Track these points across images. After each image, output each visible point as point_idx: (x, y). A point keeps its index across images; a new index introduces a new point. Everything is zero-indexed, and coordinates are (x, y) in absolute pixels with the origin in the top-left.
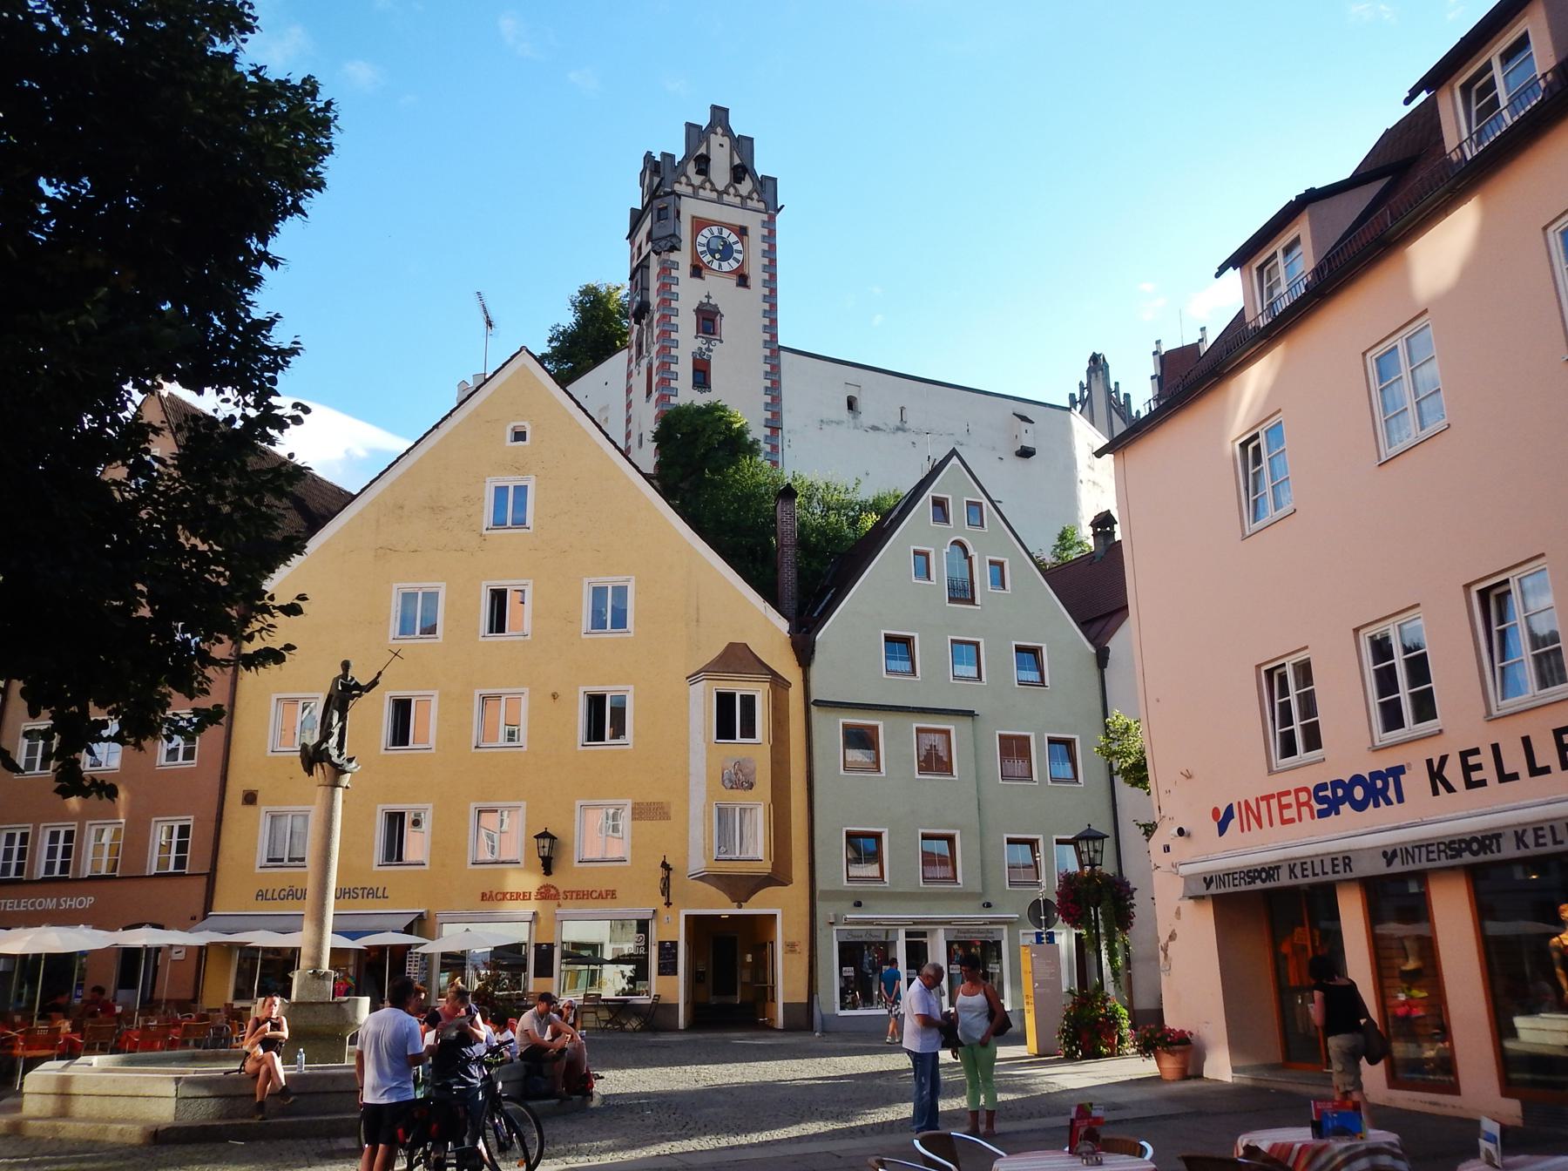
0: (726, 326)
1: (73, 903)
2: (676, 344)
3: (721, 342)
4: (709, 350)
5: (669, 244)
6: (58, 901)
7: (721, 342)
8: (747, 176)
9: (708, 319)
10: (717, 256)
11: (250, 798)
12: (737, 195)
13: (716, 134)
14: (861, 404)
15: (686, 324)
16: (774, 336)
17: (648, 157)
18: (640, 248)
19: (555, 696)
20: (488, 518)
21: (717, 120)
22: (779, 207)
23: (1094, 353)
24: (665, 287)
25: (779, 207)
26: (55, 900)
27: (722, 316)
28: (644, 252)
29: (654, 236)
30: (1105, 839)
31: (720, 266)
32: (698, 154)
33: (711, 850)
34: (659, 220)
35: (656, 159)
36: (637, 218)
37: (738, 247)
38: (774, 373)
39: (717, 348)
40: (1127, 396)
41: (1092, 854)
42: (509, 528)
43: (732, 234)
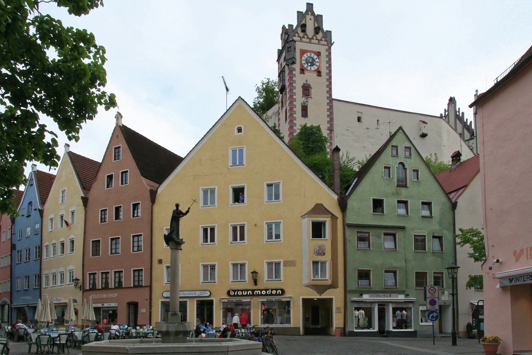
0: (313, 92)
2: (295, 106)
3: (311, 98)
4: (307, 102)
5: (292, 61)
6: (107, 295)
7: (311, 98)
8: (320, 31)
9: (306, 89)
10: (309, 64)
11: (160, 261)
12: (317, 39)
13: (308, 14)
14: (363, 119)
15: (298, 92)
16: (331, 95)
17: (284, 27)
18: (281, 64)
19: (255, 225)
20: (230, 163)
21: (309, 9)
22: (332, 43)
23: (451, 97)
24: (291, 78)
25: (332, 43)
26: (106, 295)
27: (312, 88)
28: (283, 66)
29: (286, 59)
30: (459, 269)
31: (311, 68)
32: (302, 23)
33: (310, 277)
34: (288, 52)
35: (286, 28)
36: (280, 53)
37: (317, 60)
38: (331, 107)
39: (310, 100)
40: (463, 113)
41: (453, 273)
42: (238, 165)
43: (315, 55)
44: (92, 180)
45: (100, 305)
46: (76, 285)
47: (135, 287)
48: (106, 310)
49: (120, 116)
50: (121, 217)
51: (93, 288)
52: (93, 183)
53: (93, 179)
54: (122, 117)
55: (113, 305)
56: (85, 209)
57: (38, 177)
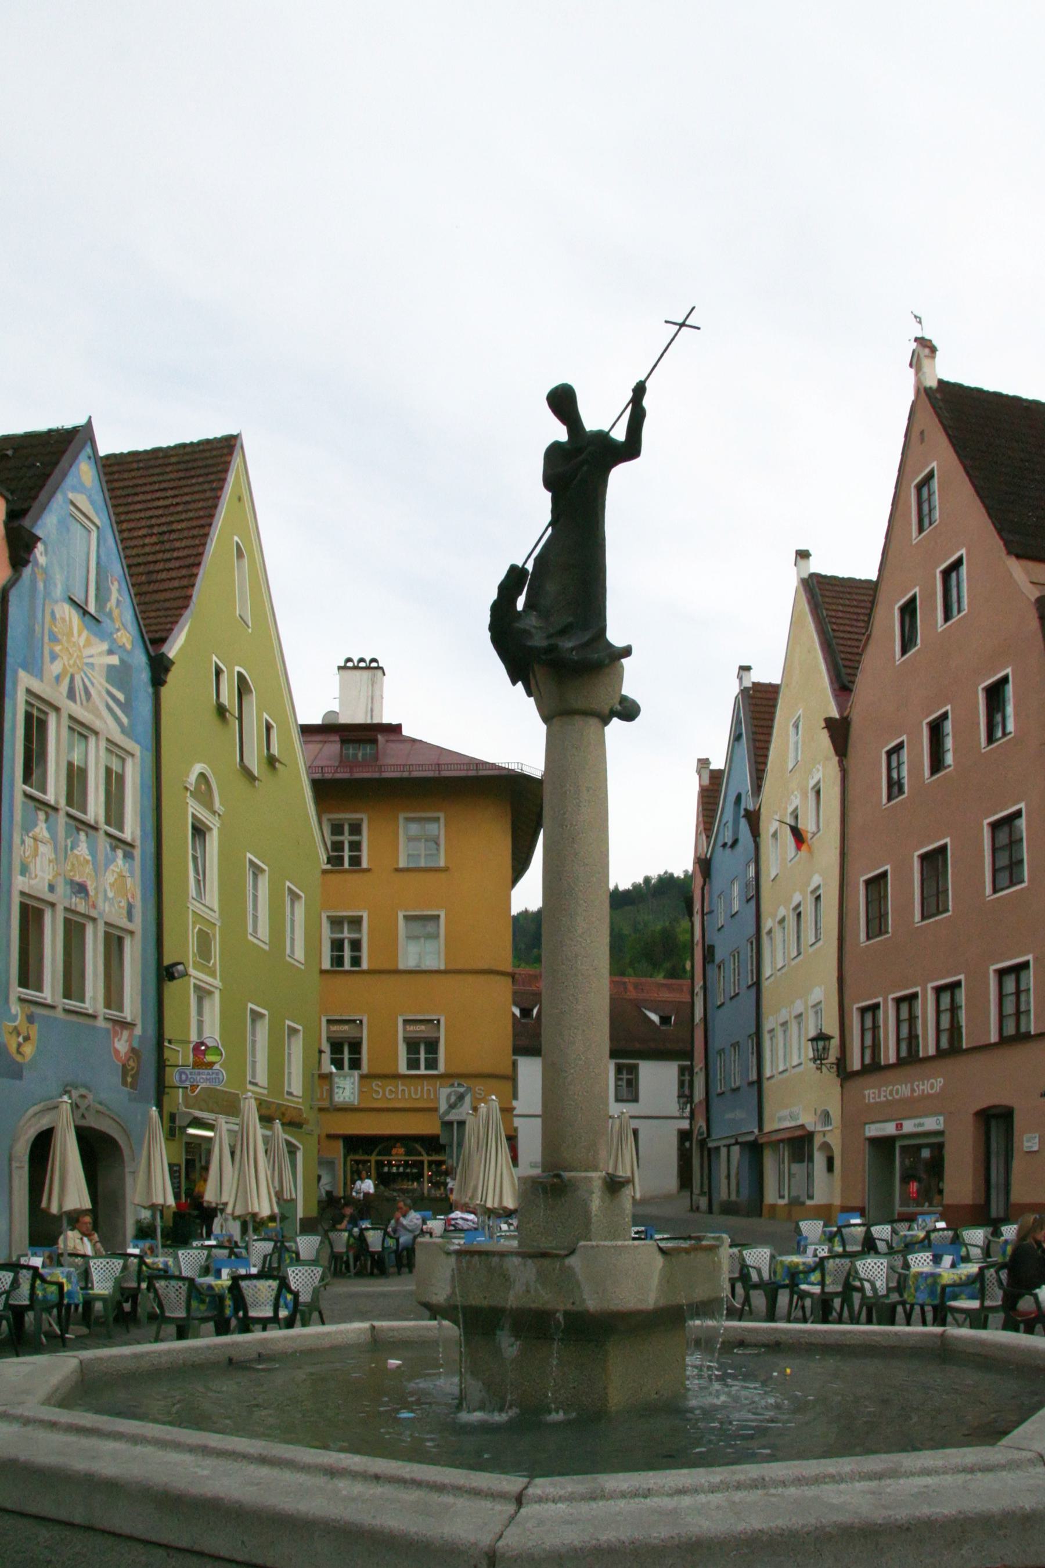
1: (925, 1087)
6: (912, 1086)
26: (909, 1085)
44: (856, 644)
45: (889, 1129)
46: (819, 1058)
47: (1004, 1041)
48: (912, 1146)
49: (927, 351)
50: (949, 758)
51: (873, 1068)
52: (861, 655)
53: (860, 637)
54: (933, 350)
55: (931, 1124)
56: (841, 763)
57: (756, 705)
